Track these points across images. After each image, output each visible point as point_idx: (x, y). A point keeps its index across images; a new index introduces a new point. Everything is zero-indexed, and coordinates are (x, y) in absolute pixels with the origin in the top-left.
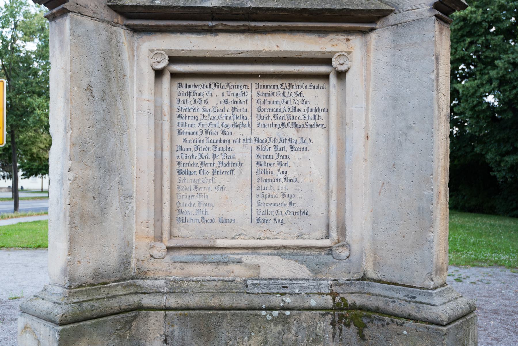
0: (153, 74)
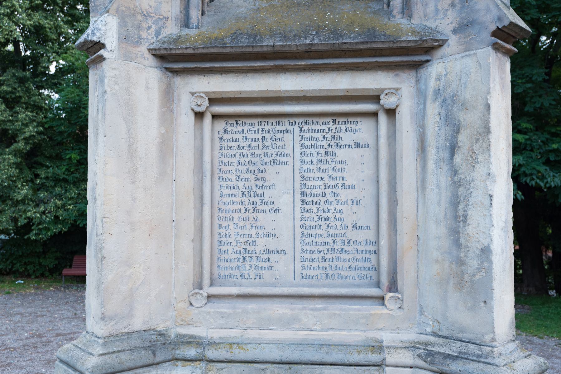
0: (192, 116)
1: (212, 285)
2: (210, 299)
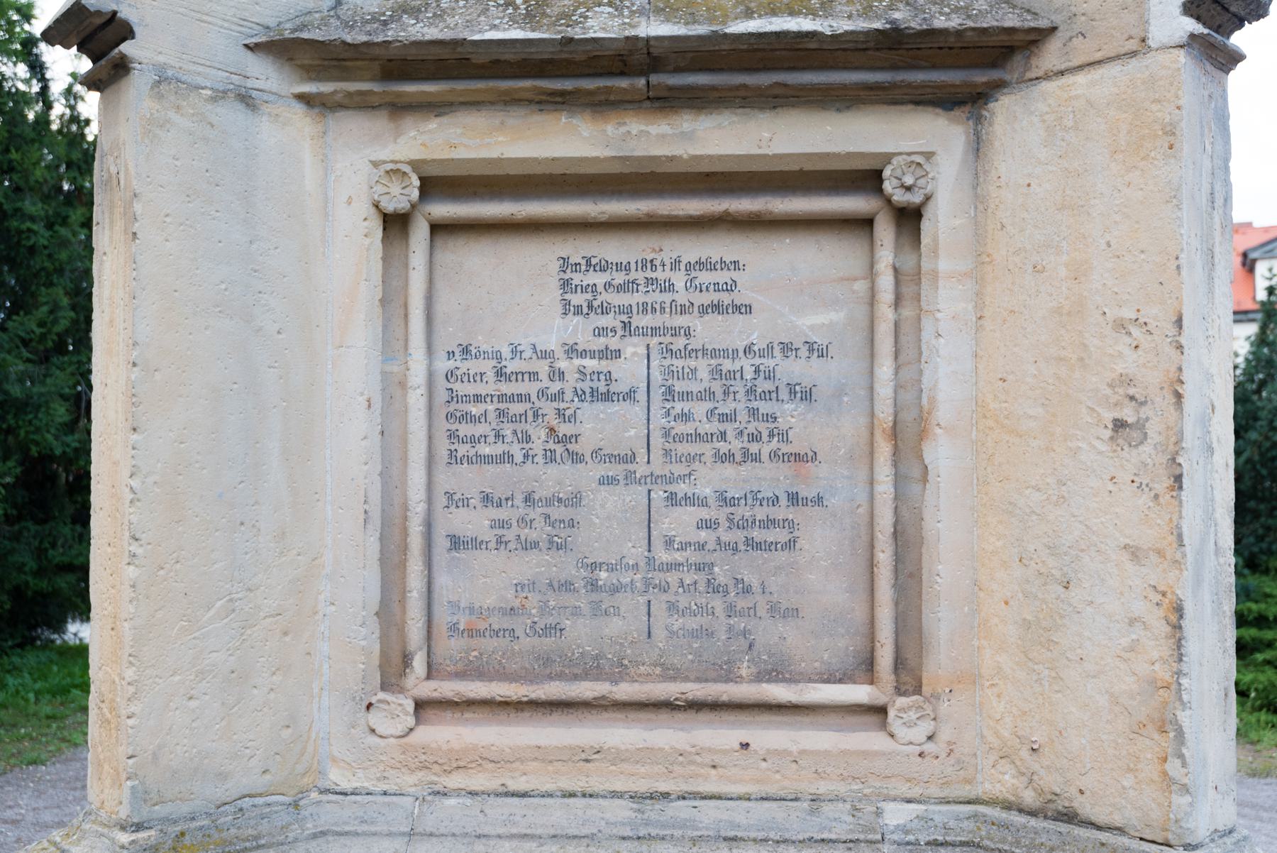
1: (429, 677)
2: (429, 713)
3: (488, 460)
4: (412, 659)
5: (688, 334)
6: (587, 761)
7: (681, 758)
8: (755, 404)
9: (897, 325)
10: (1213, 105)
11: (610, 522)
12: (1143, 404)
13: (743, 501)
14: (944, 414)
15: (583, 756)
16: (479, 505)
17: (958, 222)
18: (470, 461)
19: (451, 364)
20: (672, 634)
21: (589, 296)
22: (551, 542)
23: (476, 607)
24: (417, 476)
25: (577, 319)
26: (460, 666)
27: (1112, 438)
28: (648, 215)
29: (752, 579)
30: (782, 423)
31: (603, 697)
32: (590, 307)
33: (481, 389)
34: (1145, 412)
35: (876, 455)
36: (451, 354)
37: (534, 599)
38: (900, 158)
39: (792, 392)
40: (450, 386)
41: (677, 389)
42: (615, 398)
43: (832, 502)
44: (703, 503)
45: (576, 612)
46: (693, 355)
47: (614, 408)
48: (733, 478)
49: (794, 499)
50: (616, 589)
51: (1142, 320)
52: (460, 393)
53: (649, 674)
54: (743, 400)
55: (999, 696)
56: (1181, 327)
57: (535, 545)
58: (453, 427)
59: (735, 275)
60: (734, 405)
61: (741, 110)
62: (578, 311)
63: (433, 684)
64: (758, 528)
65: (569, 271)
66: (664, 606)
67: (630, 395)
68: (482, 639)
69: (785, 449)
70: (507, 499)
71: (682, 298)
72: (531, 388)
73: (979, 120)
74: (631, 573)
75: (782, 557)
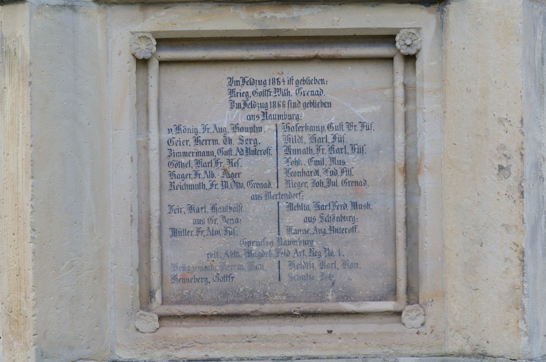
0: (133, 63)
2: (165, 322)
3: (192, 187)
4: (155, 294)
5: (297, 119)
6: (249, 342)
7: (297, 339)
8: (334, 155)
9: (406, 114)
10: (542, 17)
11: (258, 219)
12: (509, 158)
13: (328, 207)
14: (427, 161)
15: (248, 339)
16: (187, 212)
17: (433, 63)
18: (181, 188)
19: (170, 136)
20: (292, 278)
21: (244, 98)
22: (226, 231)
23: (187, 266)
24: (155, 197)
25: (237, 111)
26: (178, 298)
27: (498, 174)
28: (275, 57)
29: (333, 248)
30: (348, 166)
31: (256, 311)
32: (245, 104)
33: (187, 149)
34: (510, 162)
35: (396, 182)
36: (170, 130)
37: (217, 261)
38: (404, 30)
39: (353, 149)
40: (170, 148)
41: (292, 148)
42: (259, 153)
43: (374, 206)
44: (307, 208)
45: (240, 268)
46: (301, 129)
47: (259, 158)
48: (323, 195)
49: (355, 205)
50: (261, 255)
51: (509, 119)
52: (175, 152)
53: (280, 300)
54: (328, 153)
55: (455, 301)
56: (522, 124)
57: (218, 232)
58: (172, 170)
59: (322, 86)
60: (322, 156)
61: (323, 6)
62: (239, 106)
63: (166, 307)
64: (337, 221)
65: (233, 85)
66: (287, 264)
67: (267, 152)
68: (190, 284)
69: (350, 179)
70: (202, 208)
71: (294, 99)
72: (213, 148)
73: (443, 12)
74: (269, 246)
75: (349, 236)
